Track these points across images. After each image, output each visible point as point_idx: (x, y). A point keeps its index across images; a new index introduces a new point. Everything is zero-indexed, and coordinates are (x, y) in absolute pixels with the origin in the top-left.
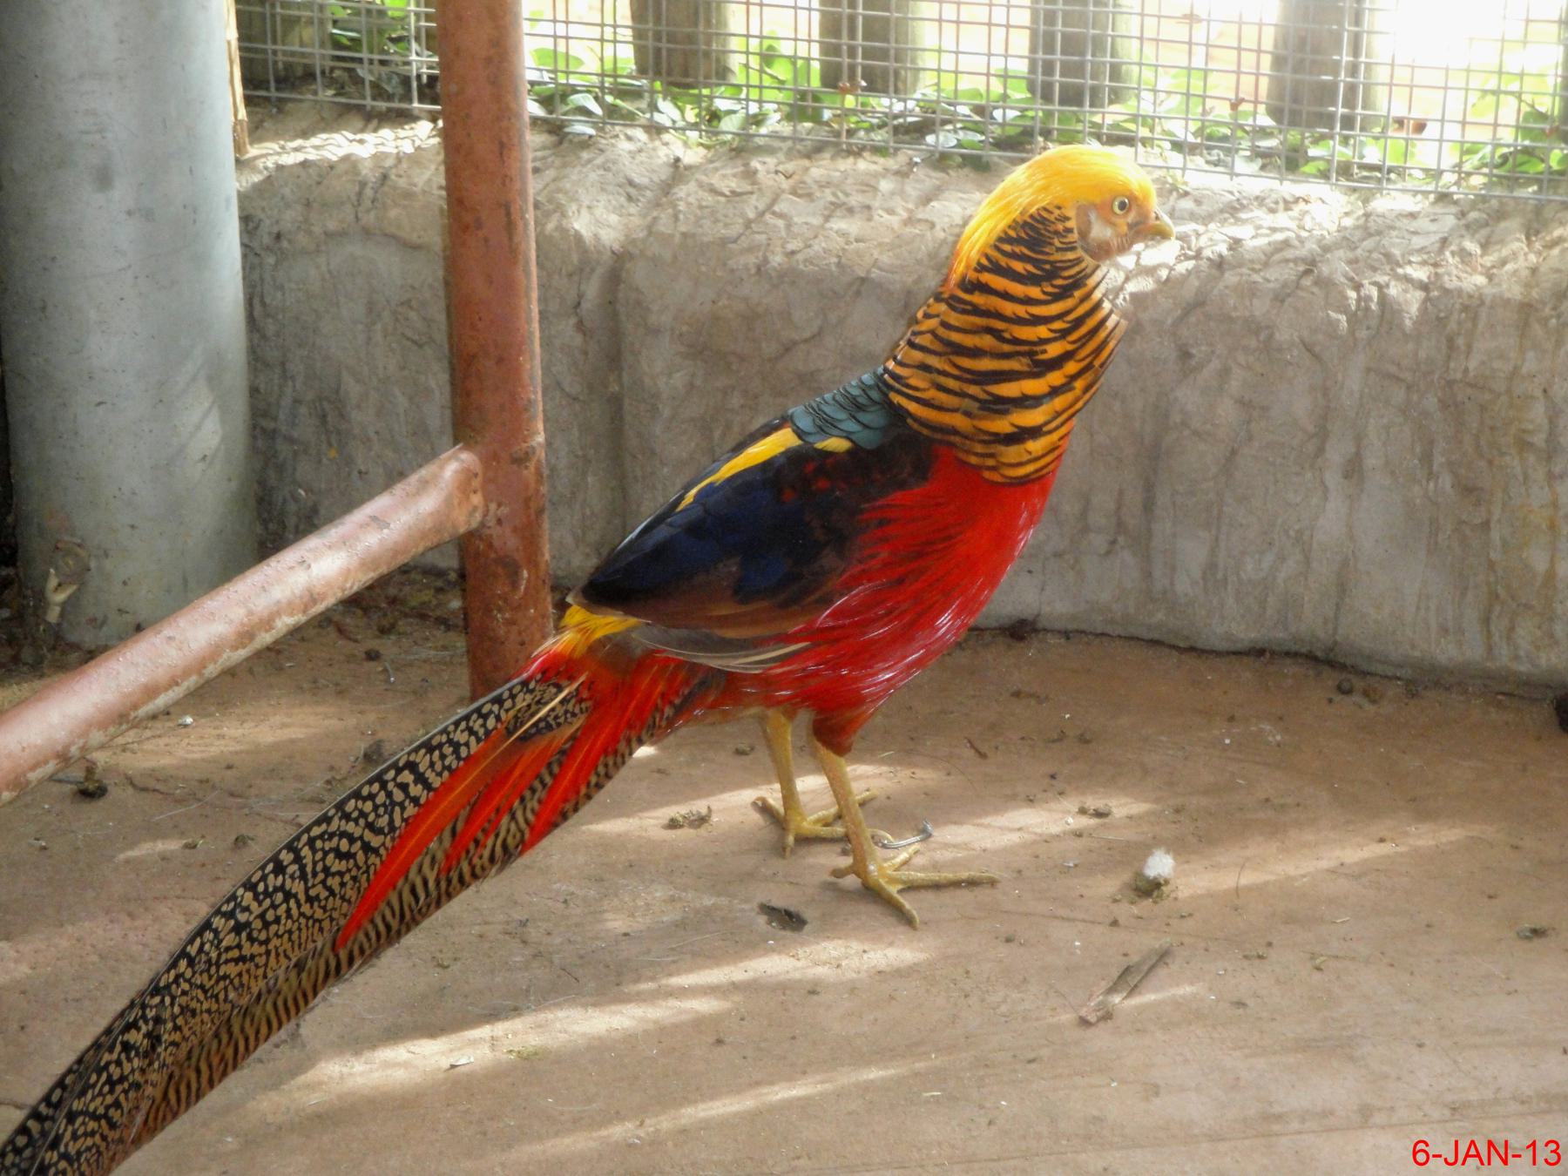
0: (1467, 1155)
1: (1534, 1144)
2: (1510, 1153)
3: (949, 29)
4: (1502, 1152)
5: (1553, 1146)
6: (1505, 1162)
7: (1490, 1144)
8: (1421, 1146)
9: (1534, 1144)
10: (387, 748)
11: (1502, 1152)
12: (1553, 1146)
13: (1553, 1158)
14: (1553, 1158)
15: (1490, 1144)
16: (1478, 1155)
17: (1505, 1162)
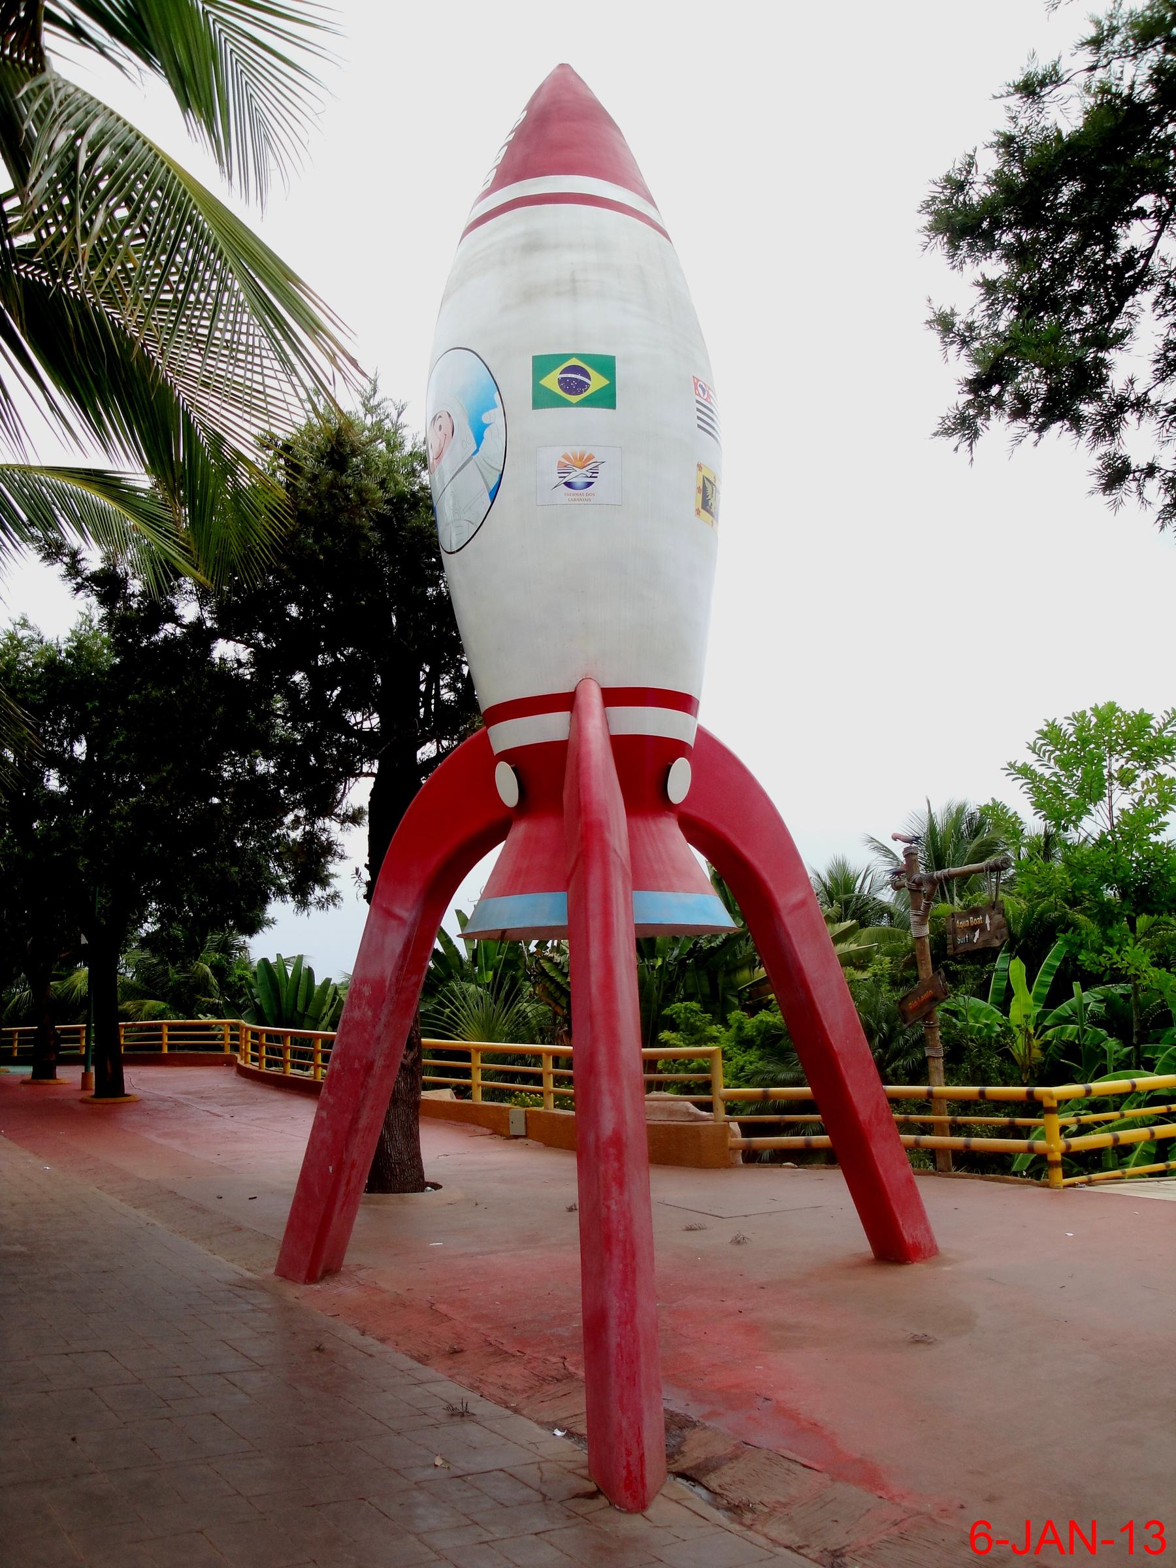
0: (1042, 1541)
1: (1130, 1525)
2: (1099, 1540)
3: (251, 343)
4: (1088, 1534)
5: (1155, 1529)
6: (1092, 1549)
7: (1073, 1525)
8: (981, 1528)
9: (1130, 1525)
10: (291, 903)
11: (1088, 1534)
12: (1155, 1529)
13: (1156, 1544)
14: (1156, 1544)
15: (1073, 1525)
16: (1057, 1541)
17: (1092, 1549)
